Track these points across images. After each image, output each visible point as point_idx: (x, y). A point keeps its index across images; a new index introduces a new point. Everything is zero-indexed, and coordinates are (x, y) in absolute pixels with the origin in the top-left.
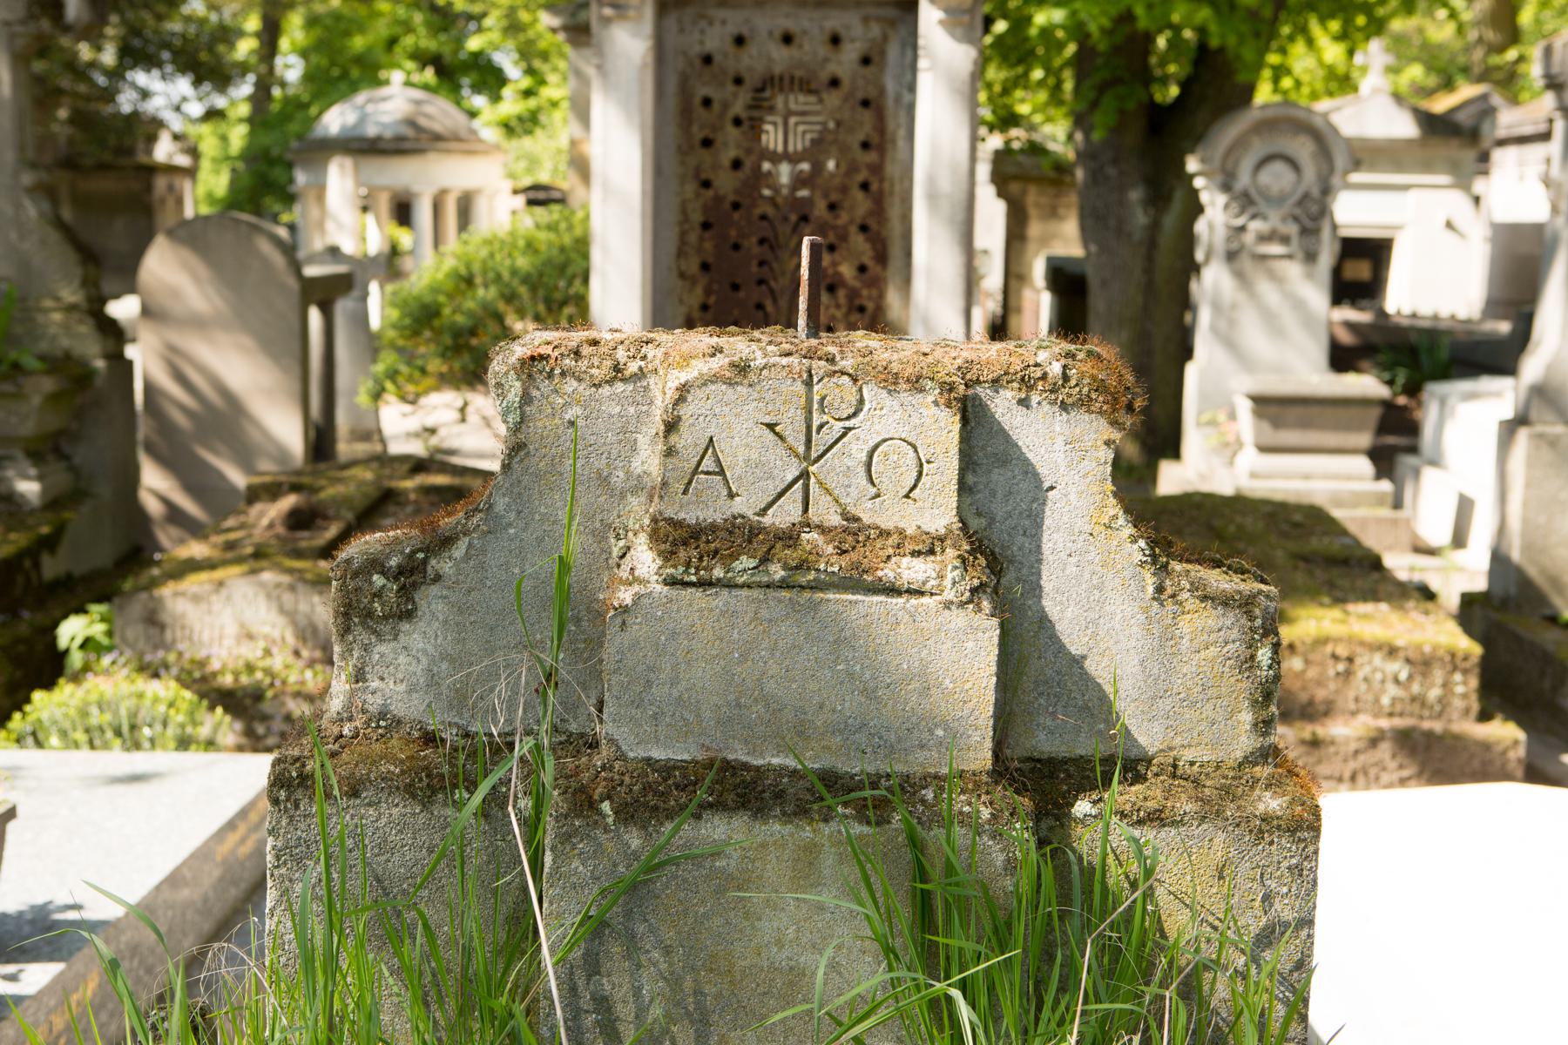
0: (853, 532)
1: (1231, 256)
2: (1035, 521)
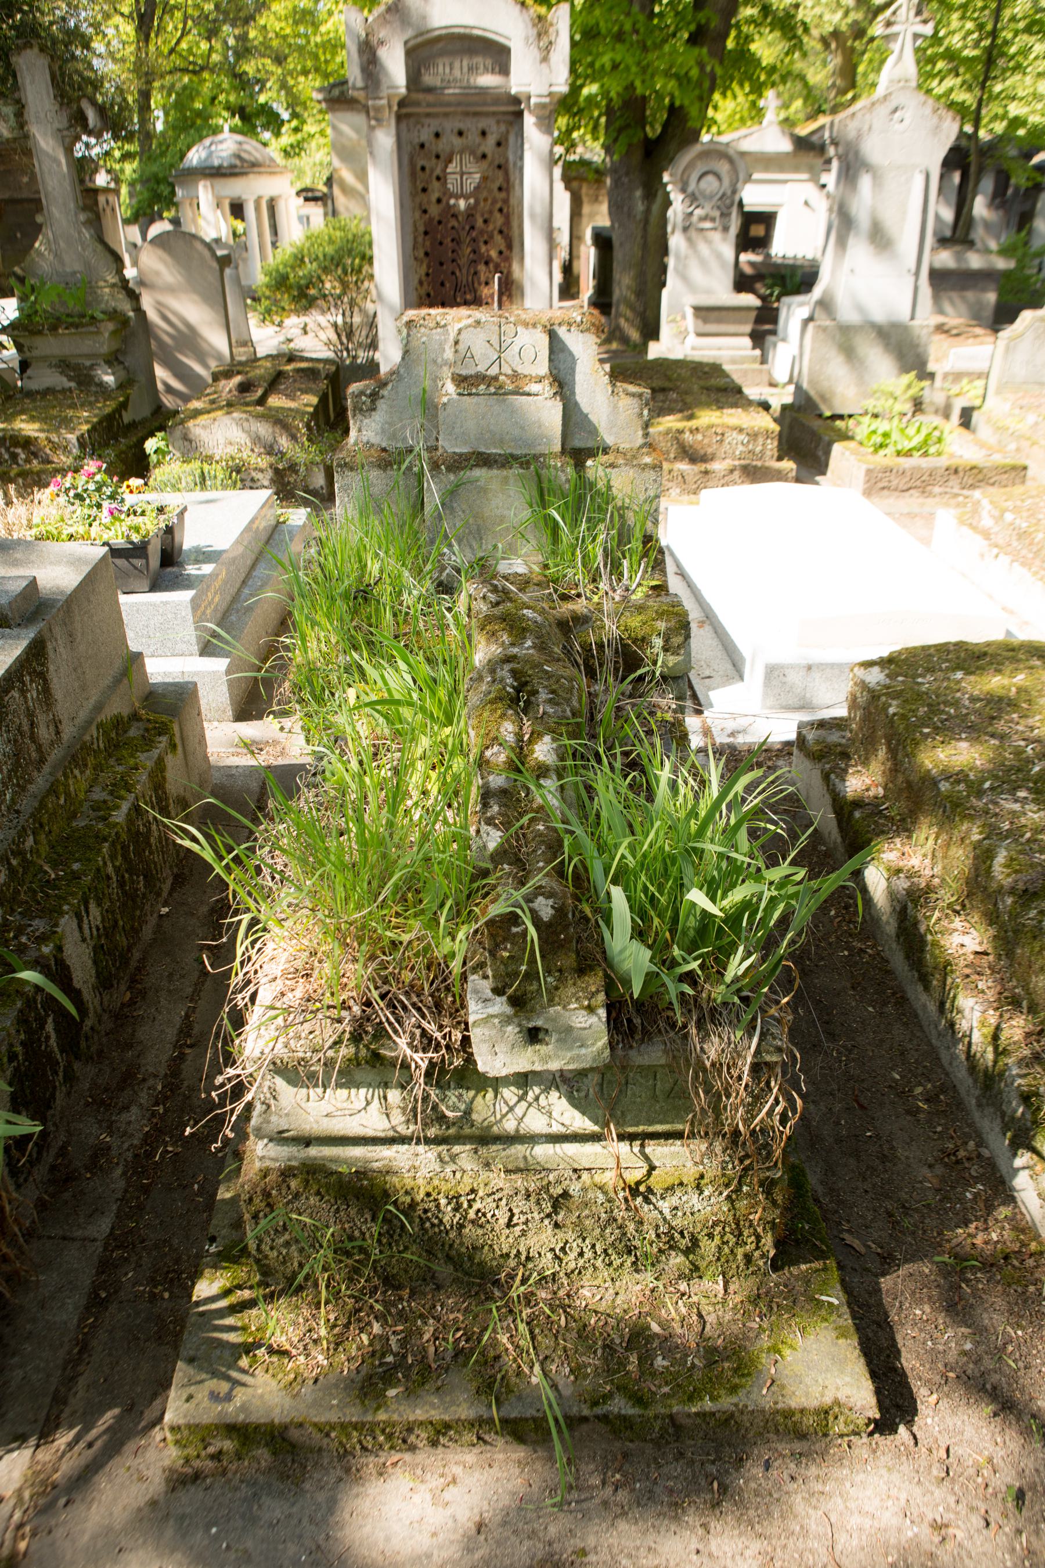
0: (515, 376)
1: (685, 229)
2: (573, 370)
